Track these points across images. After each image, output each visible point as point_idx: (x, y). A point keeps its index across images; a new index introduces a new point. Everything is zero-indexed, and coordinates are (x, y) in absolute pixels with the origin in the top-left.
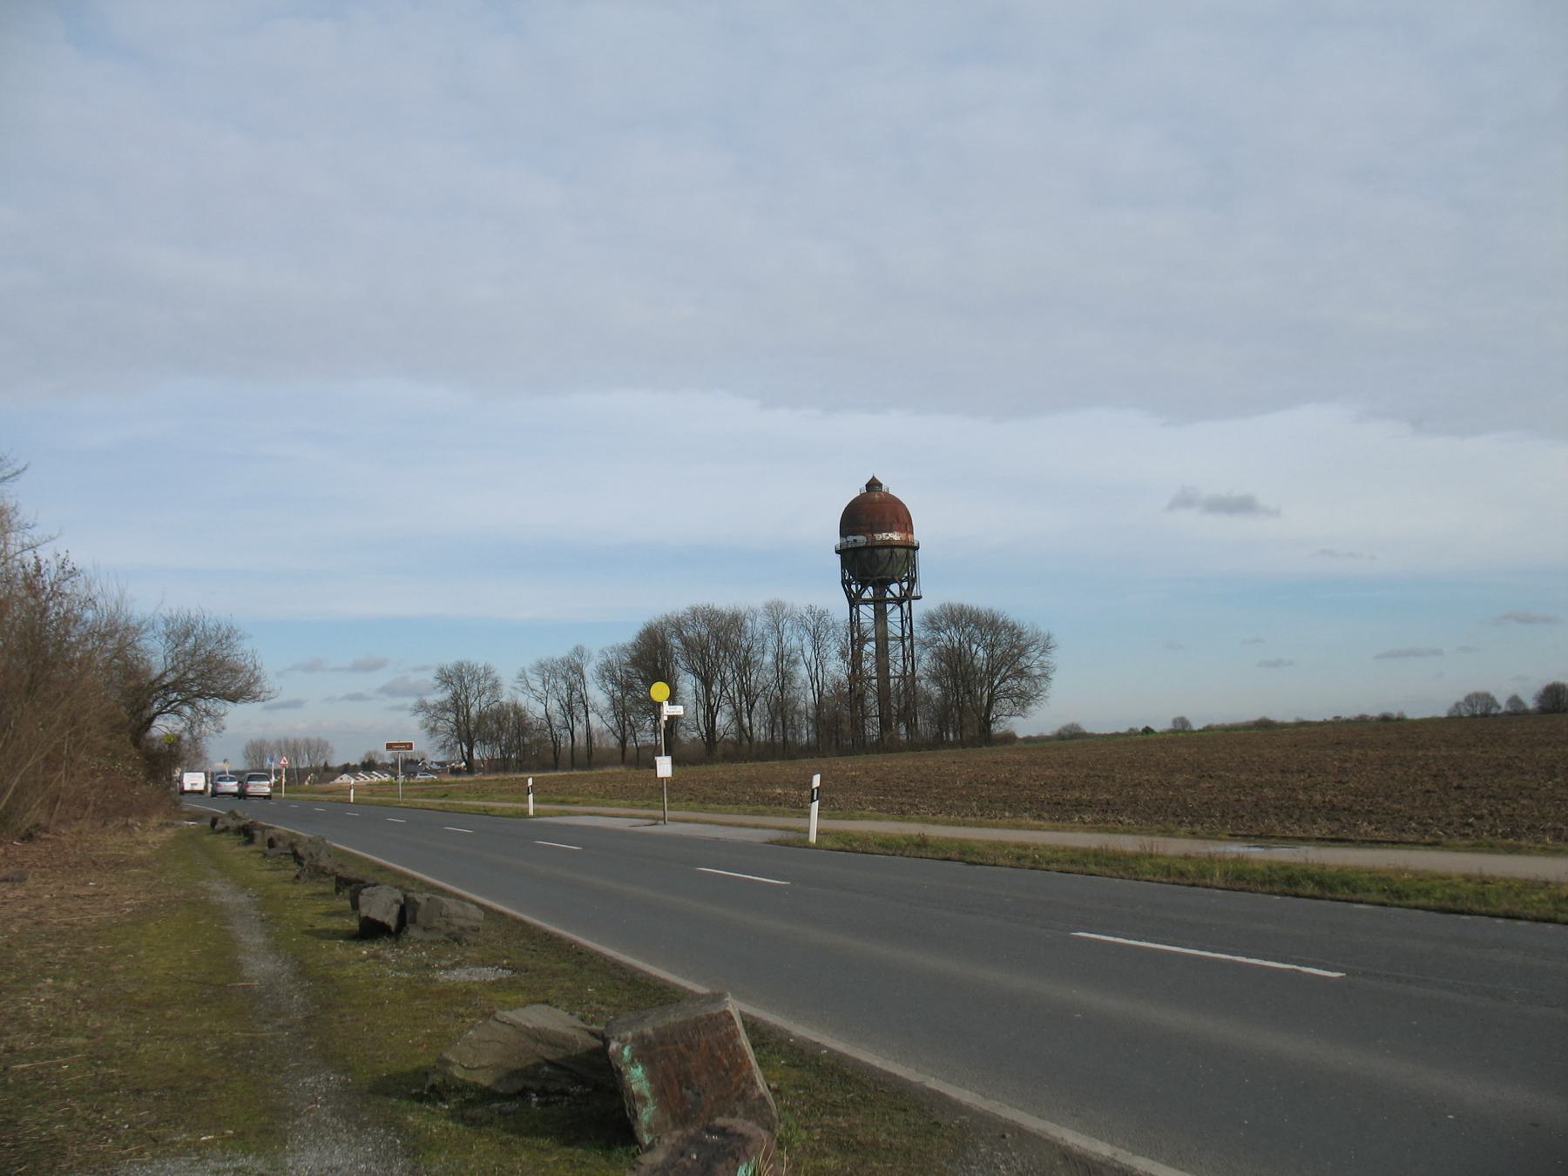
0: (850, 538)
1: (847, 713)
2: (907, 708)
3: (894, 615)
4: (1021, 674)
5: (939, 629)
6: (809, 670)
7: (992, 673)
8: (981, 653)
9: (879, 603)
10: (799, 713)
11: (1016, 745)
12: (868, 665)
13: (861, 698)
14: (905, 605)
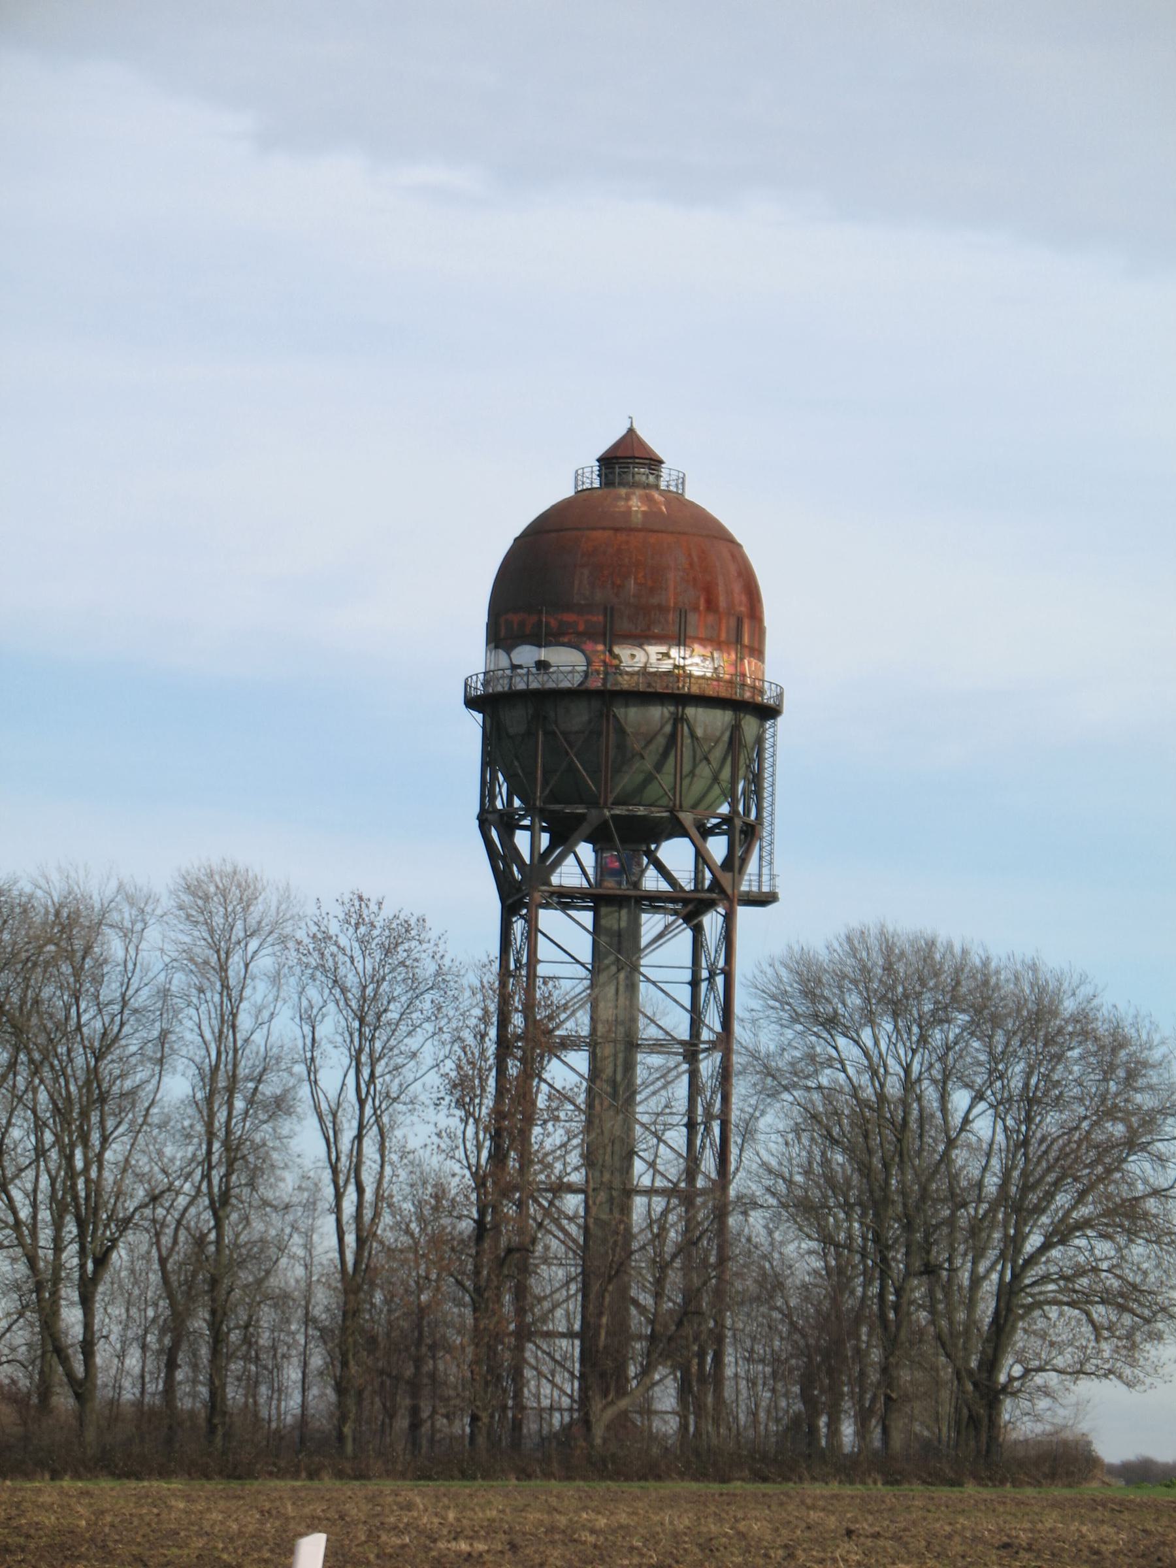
0: (526, 655)
1: (457, 1313)
2: (688, 1312)
3: (666, 953)
4: (1127, 1217)
5: (831, 1023)
6: (331, 1142)
7: (1019, 1205)
8: (983, 1126)
9: (614, 907)
10: (281, 1300)
11: (1092, 1488)
12: (556, 1139)
13: (517, 1260)
14: (712, 922)
